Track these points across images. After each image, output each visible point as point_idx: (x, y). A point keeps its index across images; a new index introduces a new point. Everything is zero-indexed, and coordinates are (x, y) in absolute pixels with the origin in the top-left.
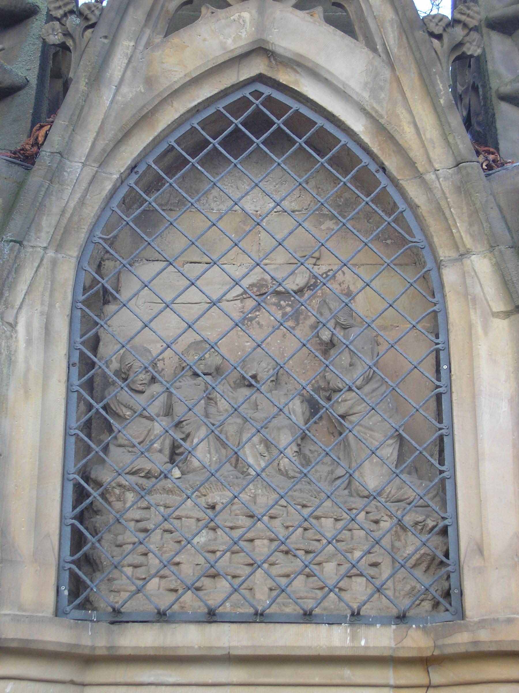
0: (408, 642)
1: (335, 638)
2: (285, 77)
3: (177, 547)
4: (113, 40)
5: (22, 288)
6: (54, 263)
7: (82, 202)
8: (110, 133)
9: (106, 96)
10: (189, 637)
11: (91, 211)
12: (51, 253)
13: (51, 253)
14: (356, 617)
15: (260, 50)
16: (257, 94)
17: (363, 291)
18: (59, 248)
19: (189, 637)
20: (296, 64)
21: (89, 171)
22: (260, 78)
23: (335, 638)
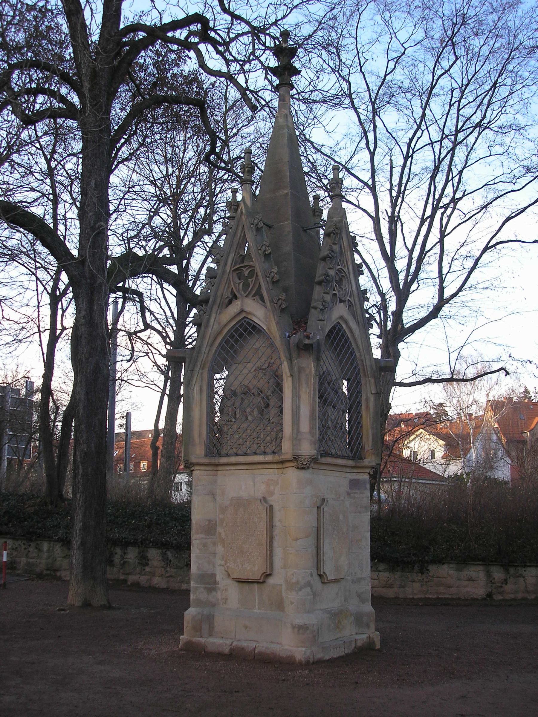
0: (275, 459)
1: (260, 458)
2: (249, 317)
3: (364, 163)
4: (210, 316)
5: (194, 381)
6: (202, 373)
7: (207, 356)
8: (212, 338)
9: (210, 330)
10: (233, 459)
11: (210, 359)
12: (201, 371)
13: (201, 371)
14: (265, 453)
15: (242, 311)
16: (245, 321)
17: (369, 166)
18: (203, 369)
19: (233, 459)
20: (250, 313)
21: (208, 349)
22: (245, 317)
23: (260, 458)
